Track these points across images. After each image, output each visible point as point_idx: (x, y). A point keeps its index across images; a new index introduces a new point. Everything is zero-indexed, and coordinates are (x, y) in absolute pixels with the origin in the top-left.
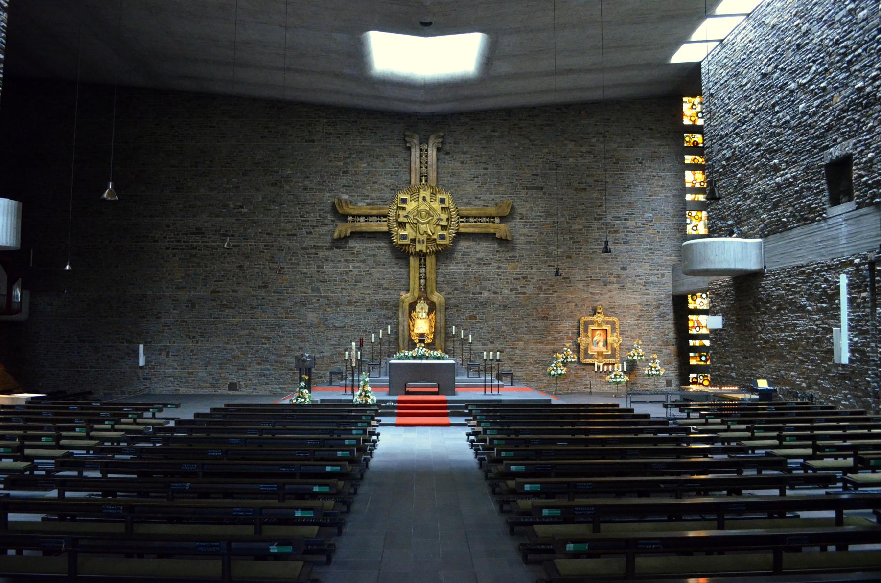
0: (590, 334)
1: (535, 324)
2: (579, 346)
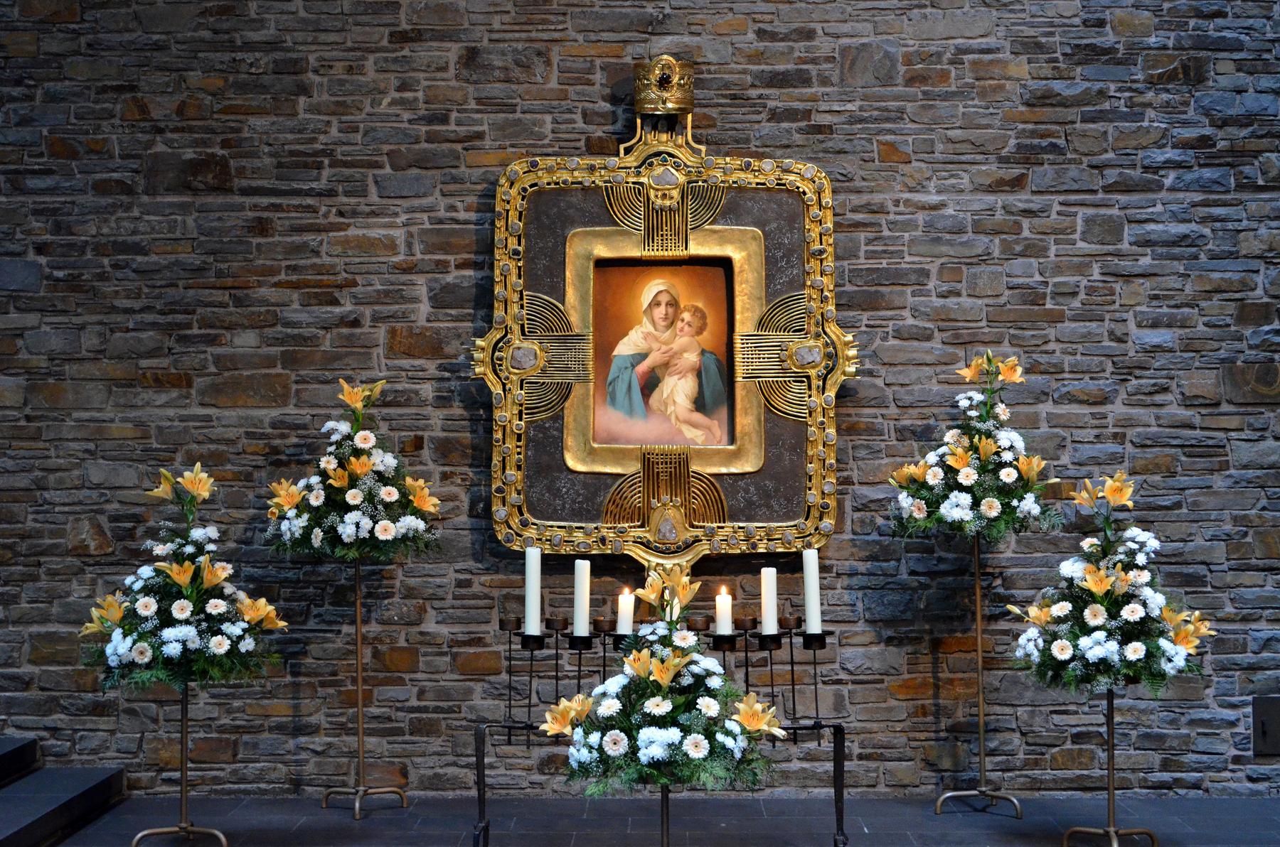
0: (576, 304)
1: (118, 227)
2: (479, 402)
